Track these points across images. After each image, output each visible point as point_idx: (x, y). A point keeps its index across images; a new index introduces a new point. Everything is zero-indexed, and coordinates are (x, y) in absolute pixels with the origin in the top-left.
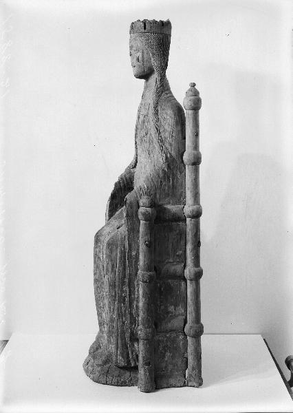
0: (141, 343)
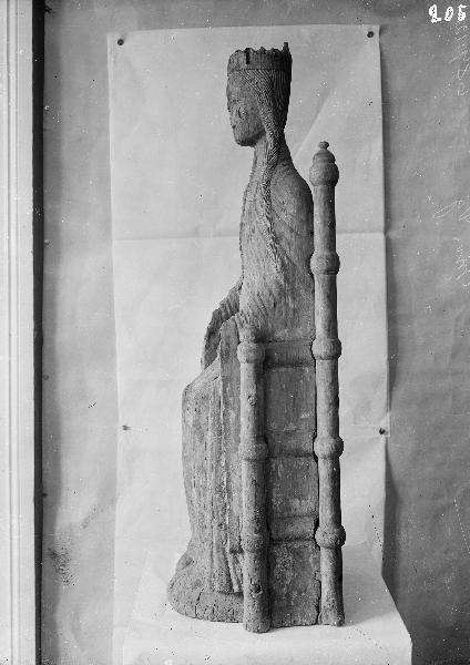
0: (246, 555)
